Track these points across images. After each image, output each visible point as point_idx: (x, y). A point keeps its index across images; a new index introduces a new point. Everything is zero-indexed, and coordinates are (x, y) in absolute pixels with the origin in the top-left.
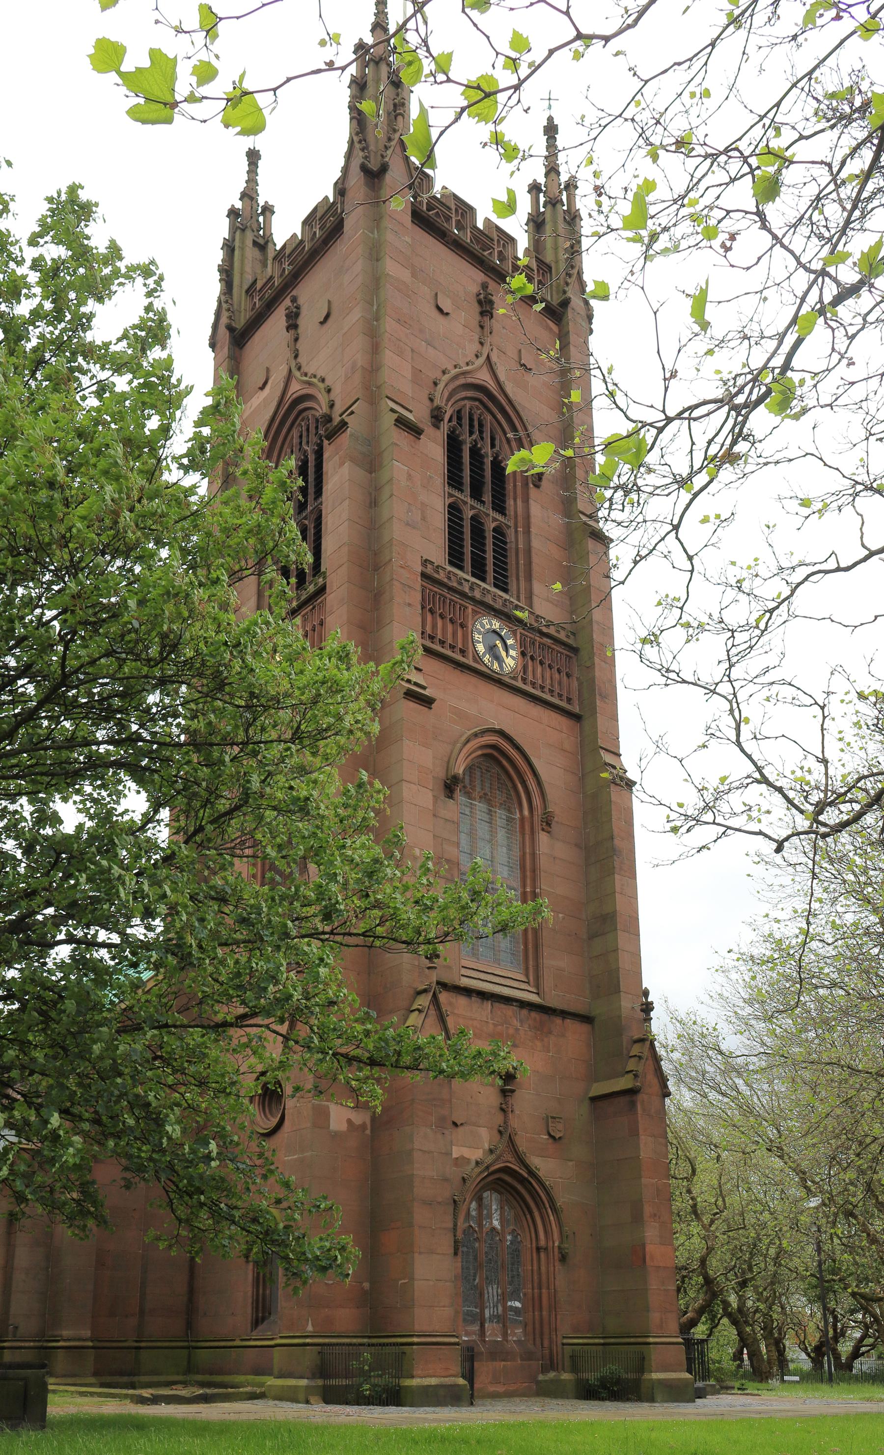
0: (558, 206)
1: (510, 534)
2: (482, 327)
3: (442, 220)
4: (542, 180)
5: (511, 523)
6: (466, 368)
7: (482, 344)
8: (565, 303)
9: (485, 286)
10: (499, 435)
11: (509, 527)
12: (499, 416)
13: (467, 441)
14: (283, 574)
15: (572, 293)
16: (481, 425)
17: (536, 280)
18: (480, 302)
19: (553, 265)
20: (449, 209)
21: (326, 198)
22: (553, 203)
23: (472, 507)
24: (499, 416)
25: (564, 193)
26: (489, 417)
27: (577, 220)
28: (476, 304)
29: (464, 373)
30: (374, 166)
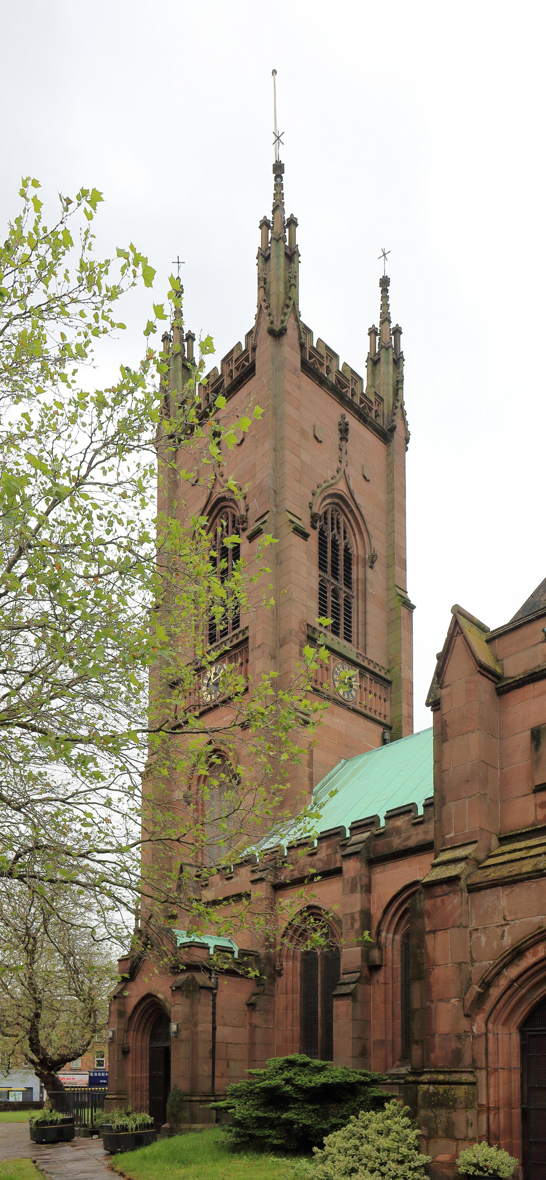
0: (281, 242)
1: (354, 601)
2: (341, 450)
3: (316, 363)
4: (270, 217)
5: (355, 594)
6: (332, 482)
7: (340, 461)
8: (393, 429)
9: (343, 417)
10: (349, 530)
11: (353, 597)
12: (349, 516)
13: (329, 535)
14: (210, 639)
15: (398, 423)
16: (338, 523)
17: (372, 408)
18: (340, 430)
19: (385, 398)
20: (371, 402)
21: (239, 344)
22: (279, 239)
23: (345, 592)
24: (349, 516)
25: (287, 230)
26: (343, 517)
27: (296, 256)
28: (338, 432)
29: (332, 485)
30: (277, 327)
